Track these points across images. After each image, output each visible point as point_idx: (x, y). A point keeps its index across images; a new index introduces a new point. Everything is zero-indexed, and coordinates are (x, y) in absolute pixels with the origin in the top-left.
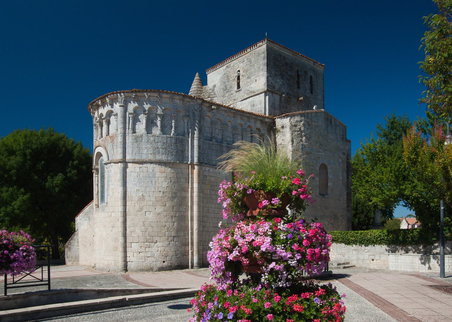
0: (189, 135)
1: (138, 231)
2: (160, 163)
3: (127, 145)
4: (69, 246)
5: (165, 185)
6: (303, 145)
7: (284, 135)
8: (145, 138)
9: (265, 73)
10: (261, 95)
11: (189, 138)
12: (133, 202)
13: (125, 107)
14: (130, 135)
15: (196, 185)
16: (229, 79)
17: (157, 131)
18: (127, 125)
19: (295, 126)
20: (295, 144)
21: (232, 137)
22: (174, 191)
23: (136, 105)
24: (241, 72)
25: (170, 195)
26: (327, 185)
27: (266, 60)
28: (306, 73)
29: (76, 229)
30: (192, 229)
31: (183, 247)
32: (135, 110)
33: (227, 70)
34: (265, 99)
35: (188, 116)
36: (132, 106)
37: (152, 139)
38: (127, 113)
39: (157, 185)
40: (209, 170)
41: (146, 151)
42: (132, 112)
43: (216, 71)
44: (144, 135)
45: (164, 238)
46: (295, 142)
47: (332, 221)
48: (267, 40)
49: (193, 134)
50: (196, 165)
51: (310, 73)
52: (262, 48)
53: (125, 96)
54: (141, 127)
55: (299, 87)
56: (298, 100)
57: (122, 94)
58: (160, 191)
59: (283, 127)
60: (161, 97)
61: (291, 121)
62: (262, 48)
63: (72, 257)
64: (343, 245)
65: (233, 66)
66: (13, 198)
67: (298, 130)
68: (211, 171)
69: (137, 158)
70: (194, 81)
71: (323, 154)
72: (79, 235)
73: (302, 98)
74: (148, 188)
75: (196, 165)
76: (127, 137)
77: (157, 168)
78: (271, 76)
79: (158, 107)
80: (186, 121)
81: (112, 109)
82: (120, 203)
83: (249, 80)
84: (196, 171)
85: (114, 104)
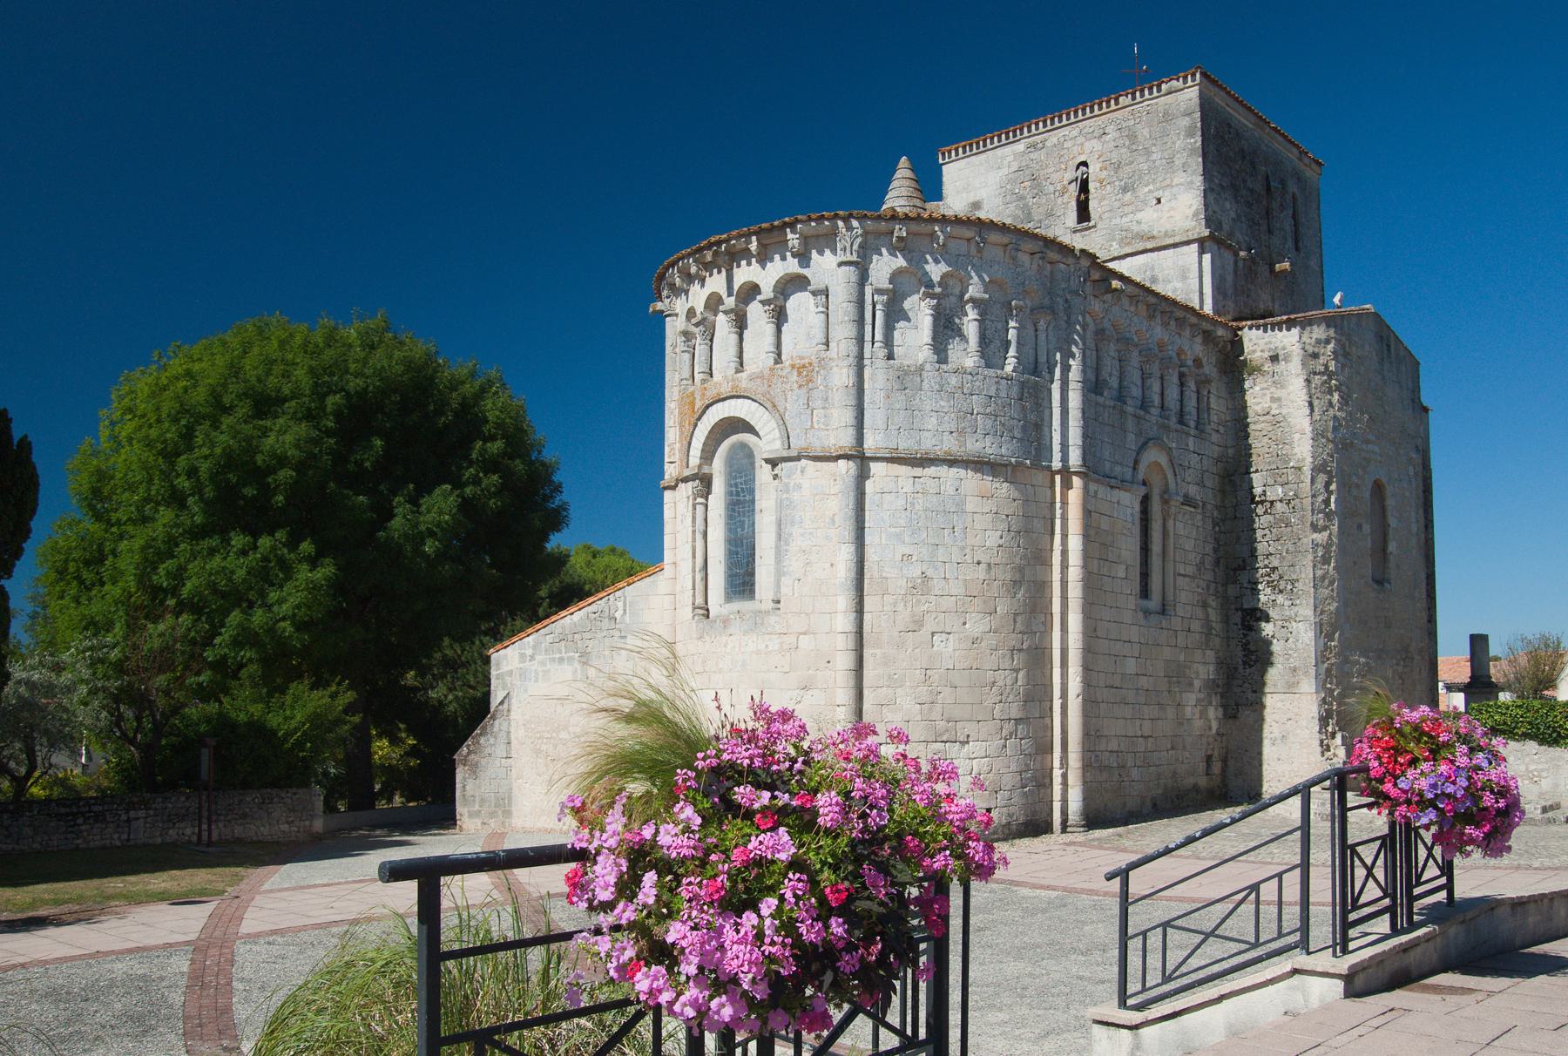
0: (1052, 373)
2: (979, 464)
3: (867, 399)
4: (472, 757)
5: (993, 539)
8: (930, 378)
9: (1198, 180)
12: (888, 599)
13: (862, 270)
15: (1075, 543)
16: (1039, 185)
17: (965, 354)
18: (868, 328)
19: (1315, 356)
20: (1317, 417)
21: (1139, 383)
22: (1017, 560)
23: (901, 262)
24: (1093, 169)
25: (1009, 577)
26: (1384, 549)
27: (1199, 139)
28: (1283, 182)
29: (497, 696)
30: (1064, 695)
31: (1039, 758)
32: (895, 276)
33: (1032, 156)
34: (1200, 263)
35: (1052, 310)
36: (884, 266)
37: (954, 380)
38: (868, 290)
39: (971, 541)
41: (934, 420)
42: (886, 285)
44: (928, 367)
45: (991, 726)
47: (1400, 669)
48: (1204, 75)
49: (1066, 369)
50: (1076, 473)
51: (1293, 188)
52: (1184, 96)
53: (866, 234)
55: (1270, 232)
56: (1272, 270)
57: (855, 223)
59: (1274, 359)
60: (984, 240)
62: (1184, 96)
63: (483, 800)
64: (1532, 745)
65: (1059, 145)
66: (269, 575)
69: (905, 444)
70: (895, 184)
71: (1377, 449)
73: (1286, 265)
74: (941, 550)
75: (1076, 473)
76: (867, 373)
77: (971, 481)
78: (1212, 190)
80: (1042, 325)
82: (843, 601)
84: (1075, 496)
85: (814, 253)
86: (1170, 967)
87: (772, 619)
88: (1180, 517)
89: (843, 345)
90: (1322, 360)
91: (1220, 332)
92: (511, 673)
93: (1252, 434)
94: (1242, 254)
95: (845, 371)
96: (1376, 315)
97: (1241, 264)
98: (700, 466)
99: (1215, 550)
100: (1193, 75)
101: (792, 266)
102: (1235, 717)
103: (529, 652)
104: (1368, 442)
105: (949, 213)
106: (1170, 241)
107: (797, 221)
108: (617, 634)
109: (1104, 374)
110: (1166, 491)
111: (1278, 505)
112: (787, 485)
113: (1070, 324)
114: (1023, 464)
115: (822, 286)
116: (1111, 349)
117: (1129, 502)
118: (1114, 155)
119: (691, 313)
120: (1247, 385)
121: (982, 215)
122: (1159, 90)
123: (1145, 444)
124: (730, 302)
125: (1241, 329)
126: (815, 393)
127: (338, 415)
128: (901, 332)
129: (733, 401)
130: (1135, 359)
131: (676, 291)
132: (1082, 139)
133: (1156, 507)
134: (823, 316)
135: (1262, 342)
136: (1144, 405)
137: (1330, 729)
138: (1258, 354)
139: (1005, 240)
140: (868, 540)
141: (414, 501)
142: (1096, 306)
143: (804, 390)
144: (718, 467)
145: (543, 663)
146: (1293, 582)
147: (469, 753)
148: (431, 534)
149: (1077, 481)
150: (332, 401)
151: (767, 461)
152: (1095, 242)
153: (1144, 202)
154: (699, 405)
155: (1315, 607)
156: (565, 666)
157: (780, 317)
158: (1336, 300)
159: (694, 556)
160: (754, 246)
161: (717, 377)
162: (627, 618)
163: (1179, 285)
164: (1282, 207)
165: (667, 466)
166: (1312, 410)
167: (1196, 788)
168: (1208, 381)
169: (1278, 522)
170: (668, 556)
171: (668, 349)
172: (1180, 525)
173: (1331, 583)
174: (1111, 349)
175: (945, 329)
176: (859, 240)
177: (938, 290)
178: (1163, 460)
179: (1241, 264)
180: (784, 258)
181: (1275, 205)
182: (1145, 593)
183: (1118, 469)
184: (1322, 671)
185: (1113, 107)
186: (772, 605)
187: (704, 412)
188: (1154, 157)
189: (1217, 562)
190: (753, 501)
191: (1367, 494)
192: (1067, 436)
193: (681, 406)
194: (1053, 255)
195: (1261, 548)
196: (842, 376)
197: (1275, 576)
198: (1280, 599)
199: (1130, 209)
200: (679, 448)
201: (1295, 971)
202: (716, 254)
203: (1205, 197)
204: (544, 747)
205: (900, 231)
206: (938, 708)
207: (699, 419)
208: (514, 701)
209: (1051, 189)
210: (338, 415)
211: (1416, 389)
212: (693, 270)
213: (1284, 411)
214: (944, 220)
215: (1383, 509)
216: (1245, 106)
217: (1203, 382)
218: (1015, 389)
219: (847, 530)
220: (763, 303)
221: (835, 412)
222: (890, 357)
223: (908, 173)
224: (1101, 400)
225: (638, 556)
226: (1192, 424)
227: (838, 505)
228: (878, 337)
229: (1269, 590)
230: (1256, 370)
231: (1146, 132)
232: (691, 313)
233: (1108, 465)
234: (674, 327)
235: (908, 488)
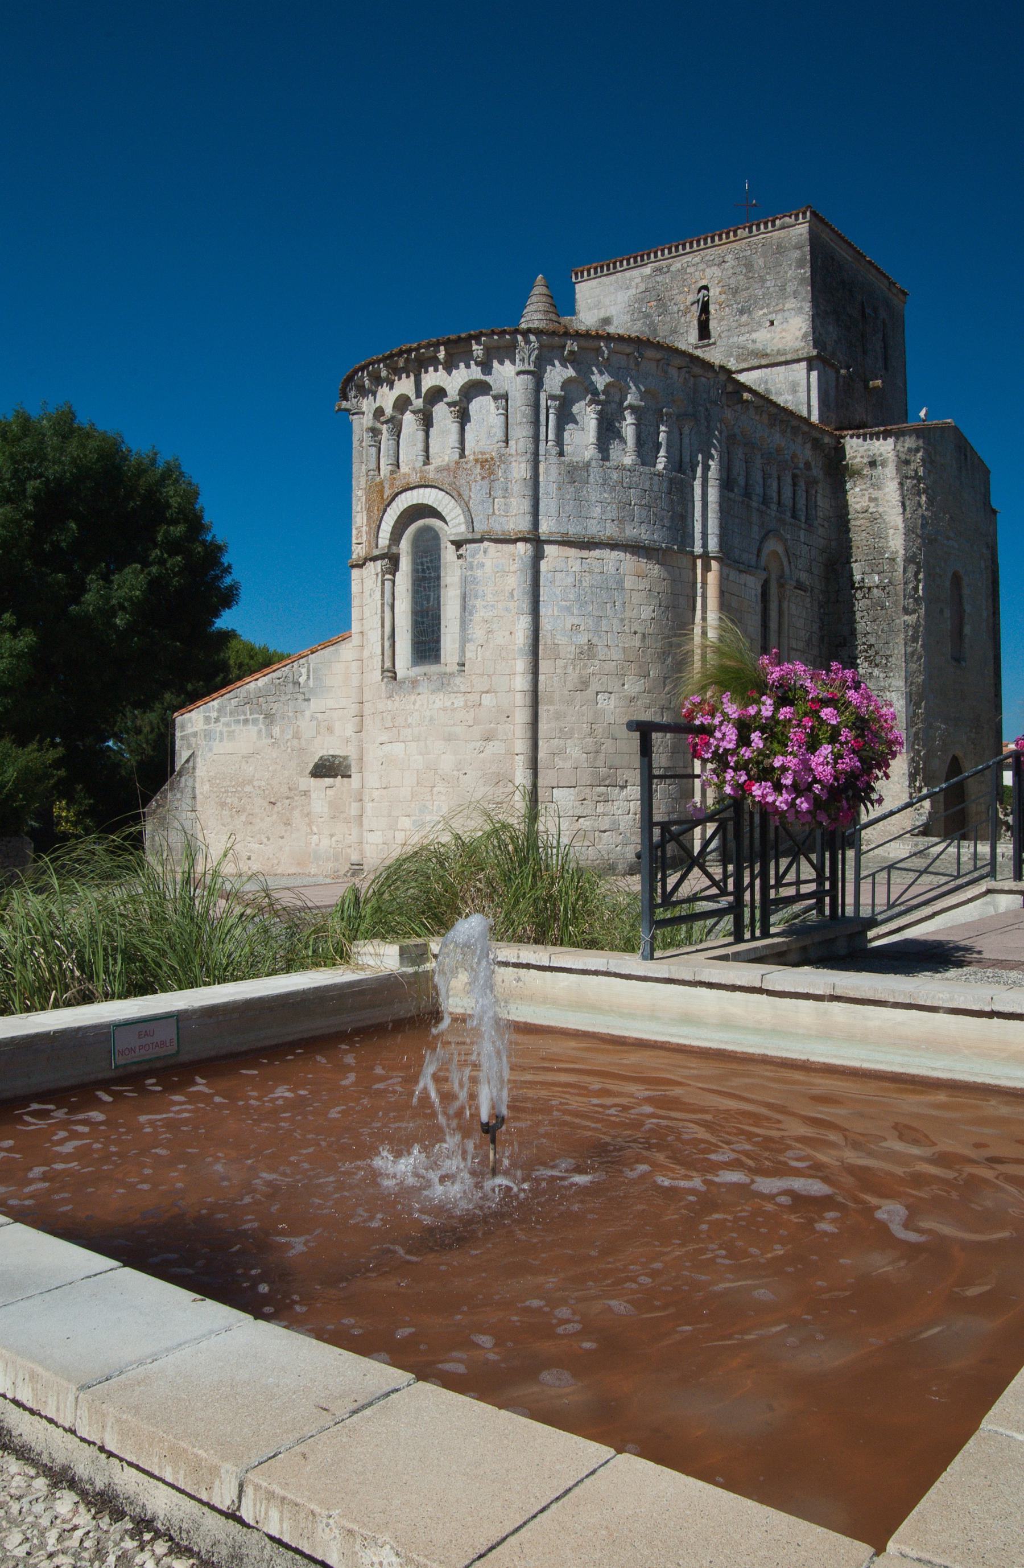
0: (694, 471)
1: (575, 752)
2: (635, 548)
3: (541, 491)
5: (647, 612)
6: (923, 515)
7: (877, 486)
9: (807, 306)
10: (795, 366)
11: (694, 479)
12: (560, 663)
14: (553, 459)
16: (664, 305)
17: (625, 455)
18: (543, 429)
19: (907, 462)
21: (761, 481)
23: (570, 372)
24: (714, 292)
27: (808, 270)
29: (182, 755)
32: (566, 384)
33: (658, 279)
36: (557, 375)
37: (615, 476)
38: (543, 396)
41: (598, 510)
42: (558, 392)
43: (613, 278)
44: (594, 463)
46: (908, 509)
47: (973, 736)
48: (813, 213)
49: (706, 468)
50: (714, 558)
52: (801, 230)
53: (541, 348)
54: (583, 436)
55: (865, 353)
56: (866, 386)
57: (532, 338)
58: (635, 633)
59: (873, 464)
60: (641, 356)
61: (898, 448)
65: (683, 270)
67: (913, 474)
69: (574, 530)
72: (198, 773)
74: (604, 622)
75: (714, 558)
76: (542, 467)
77: (629, 562)
79: (631, 384)
80: (686, 430)
81: (487, 378)
82: (521, 665)
83: (744, 318)
84: (712, 577)
86: (892, 901)
87: (458, 680)
89: (522, 443)
90: (913, 466)
91: (827, 440)
92: (195, 734)
93: (853, 529)
94: (843, 371)
95: (523, 465)
96: (956, 428)
97: (841, 380)
98: (389, 547)
99: (821, 629)
100: (804, 213)
101: (475, 373)
103: (214, 715)
104: (948, 538)
105: (583, 328)
106: (782, 359)
107: (481, 334)
108: (301, 697)
110: (781, 576)
111: (875, 590)
112: (471, 563)
113: (709, 430)
114: (669, 549)
115: (502, 392)
116: (739, 453)
117: (753, 583)
118: (732, 281)
119: (379, 412)
120: (848, 486)
121: (611, 330)
122: (773, 225)
123: (767, 534)
124: (418, 403)
125: (844, 437)
126: (496, 484)
127: (36, 498)
128: (570, 434)
129: (421, 490)
130: (758, 462)
131: (363, 392)
132: (704, 268)
133: (773, 590)
135: (862, 449)
136: (765, 501)
137: (918, 784)
138: (858, 459)
139: (659, 356)
140: (542, 611)
141: (106, 578)
142: (728, 414)
143: (486, 482)
144: (405, 546)
145: (228, 725)
146: (887, 657)
147: (158, 806)
148: (122, 607)
149: (714, 564)
150: (32, 486)
151: (453, 542)
152: (715, 356)
153: (760, 324)
154: (388, 493)
155: (906, 679)
156: (250, 727)
157: (463, 418)
158: (922, 414)
159: (383, 626)
160: (442, 355)
161: (404, 469)
162: (311, 683)
163: (790, 398)
165: (354, 547)
166: (904, 510)
168: (816, 482)
169: (874, 605)
170: (355, 627)
171: (355, 444)
172: (793, 607)
173: (919, 659)
174: (739, 453)
175: (608, 432)
176: (536, 352)
177: (602, 397)
178: (780, 550)
179: (841, 380)
180: (468, 366)
183: (745, 556)
184: (912, 735)
185: (732, 238)
187: (393, 499)
188: (768, 284)
189: (822, 639)
190: (439, 578)
191: (948, 584)
192: (707, 527)
193: (368, 491)
194: (697, 370)
195: (860, 627)
196: (520, 470)
197: (871, 652)
198: (876, 672)
199: (746, 329)
200: (366, 530)
201: (989, 891)
202: (407, 360)
203: (813, 321)
204: (229, 800)
205: (572, 346)
206: (602, 756)
207: (388, 505)
208: (199, 760)
209: (675, 308)
210: (36, 498)
211: (987, 494)
212: (384, 373)
213: (881, 510)
214: (578, 335)
215: (960, 597)
216: (846, 242)
217: (811, 483)
218: (665, 484)
219: (526, 605)
220: (449, 405)
221: (514, 501)
222: (561, 454)
223: (544, 290)
224: (732, 495)
225: (334, 624)
226: (803, 519)
227: (516, 581)
228: (551, 437)
229: (866, 664)
230: (857, 473)
231: (761, 262)
232: (379, 412)
234: (361, 424)
235: (577, 567)
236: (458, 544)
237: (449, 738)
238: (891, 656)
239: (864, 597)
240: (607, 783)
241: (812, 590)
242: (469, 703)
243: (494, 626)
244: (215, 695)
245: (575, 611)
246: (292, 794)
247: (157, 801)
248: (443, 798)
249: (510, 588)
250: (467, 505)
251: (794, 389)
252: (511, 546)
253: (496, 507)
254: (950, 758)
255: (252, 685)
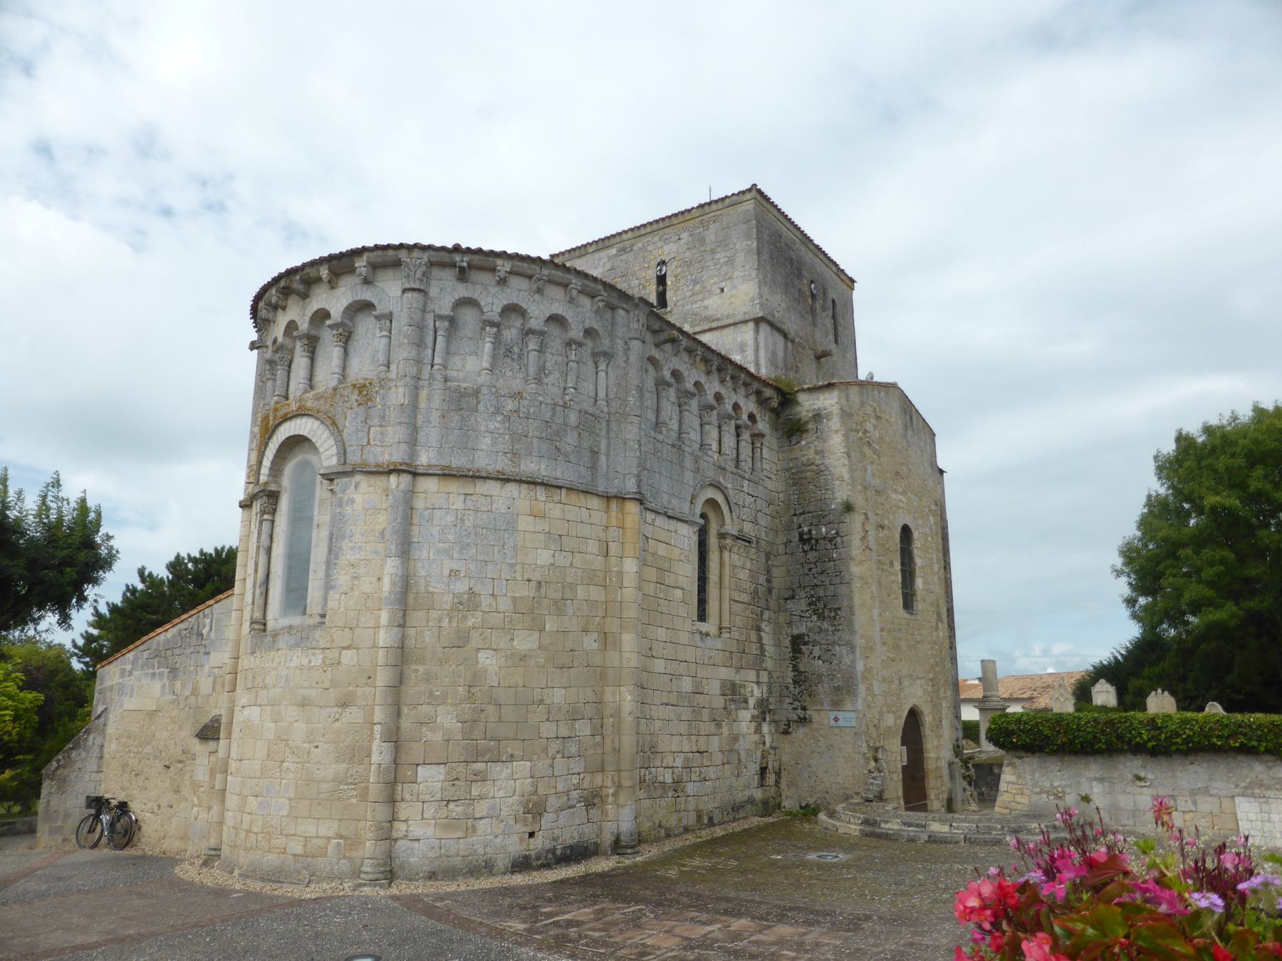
1: (447, 719)
10: (743, 328)
21: (698, 428)
40: (654, 520)
41: (488, 441)
63: (67, 816)
65: (644, 249)
68: (657, 523)
69: (457, 462)
72: (110, 730)
76: (423, 394)
83: (698, 287)
87: (318, 633)
88: (735, 549)
92: (111, 688)
102: (786, 732)
103: (128, 667)
108: (202, 650)
109: (664, 416)
112: (341, 499)
115: (386, 311)
133: (713, 542)
134: (385, 340)
147: (59, 767)
164: (824, 308)
167: (751, 801)
181: (818, 306)
182: (702, 616)
186: (319, 619)
196: (398, 395)
197: (820, 605)
198: (825, 625)
208: (111, 715)
211: (934, 455)
233: (665, 497)
236: (330, 477)
237: (304, 703)
238: (839, 609)
239: (812, 549)
240: (486, 758)
241: (757, 542)
242: (328, 662)
243: (362, 571)
244: (131, 647)
245: (455, 555)
246: (183, 758)
247: (58, 761)
248: (291, 776)
249: (380, 527)
250: (340, 432)
251: (742, 349)
252: (384, 478)
253: (371, 436)
254: (906, 713)
255: (162, 637)
